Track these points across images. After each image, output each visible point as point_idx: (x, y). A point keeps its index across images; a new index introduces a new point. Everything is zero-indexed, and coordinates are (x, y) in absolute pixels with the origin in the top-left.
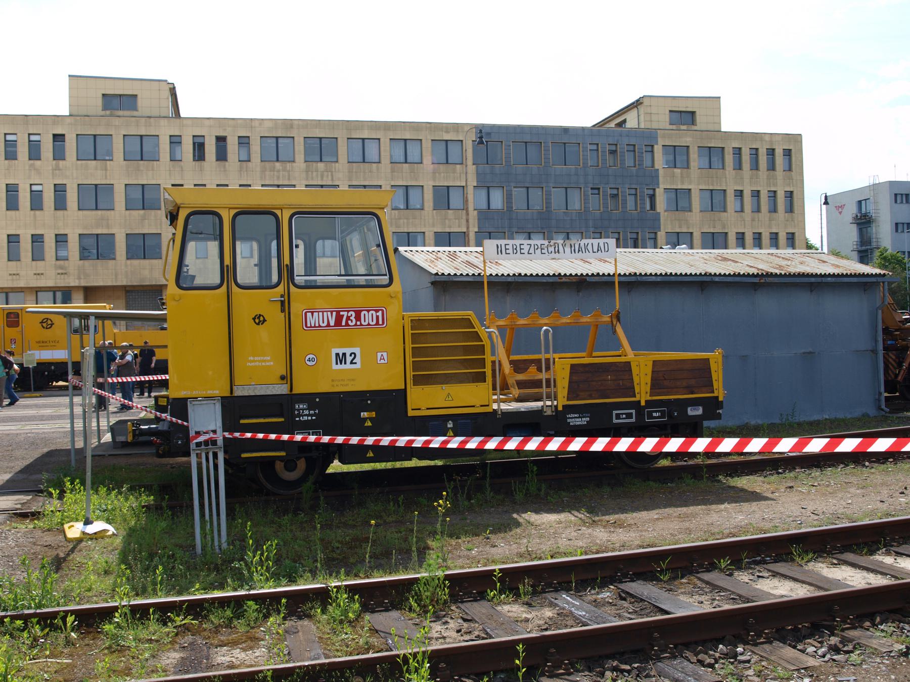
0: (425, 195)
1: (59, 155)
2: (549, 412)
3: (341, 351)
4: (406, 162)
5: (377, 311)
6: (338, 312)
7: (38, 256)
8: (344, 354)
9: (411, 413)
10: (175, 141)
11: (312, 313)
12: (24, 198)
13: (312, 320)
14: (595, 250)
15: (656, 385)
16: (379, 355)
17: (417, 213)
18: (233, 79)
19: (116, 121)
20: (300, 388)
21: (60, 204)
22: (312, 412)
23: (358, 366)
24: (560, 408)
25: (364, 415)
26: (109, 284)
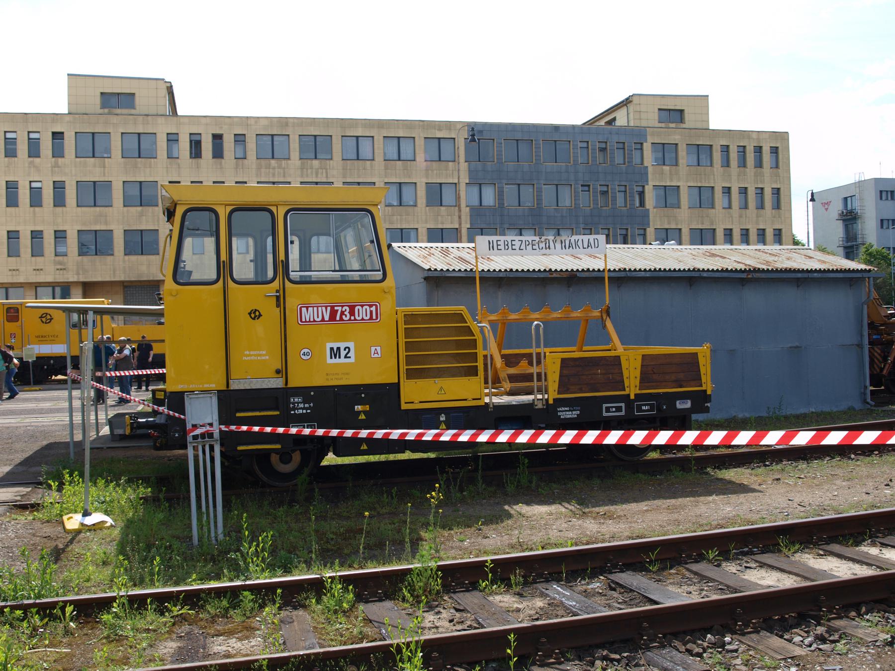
0: (418, 192)
1: (58, 152)
2: (540, 406)
3: (335, 346)
4: (399, 160)
5: (371, 306)
6: (332, 307)
7: (37, 251)
8: (339, 349)
9: (404, 407)
10: (172, 139)
11: (307, 308)
12: (24, 195)
13: (307, 315)
14: (586, 246)
15: (645, 379)
16: (373, 349)
17: (410, 209)
18: (229, 78)
19: (114, 119)
20: (295, 382)
21: (59, 201)
22: (307, 405)
23: (352, 360)
24: (551, 402)
25: (358, 408)
26: (108, 279)
